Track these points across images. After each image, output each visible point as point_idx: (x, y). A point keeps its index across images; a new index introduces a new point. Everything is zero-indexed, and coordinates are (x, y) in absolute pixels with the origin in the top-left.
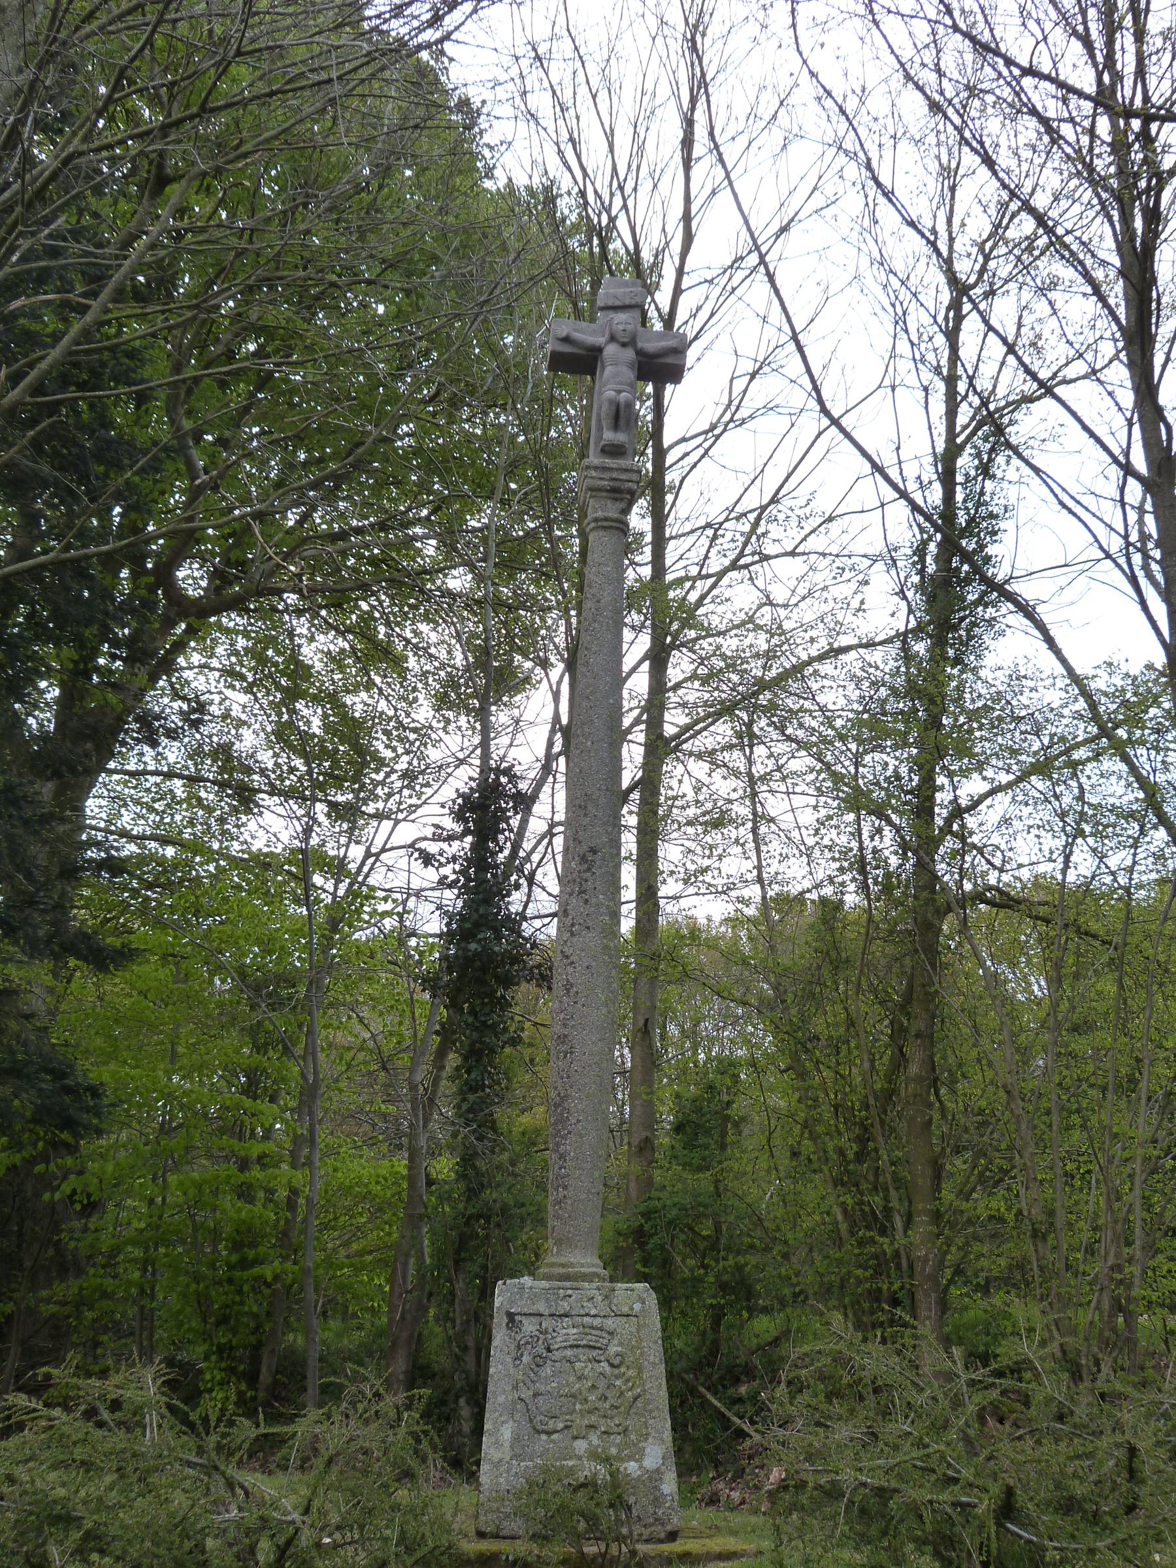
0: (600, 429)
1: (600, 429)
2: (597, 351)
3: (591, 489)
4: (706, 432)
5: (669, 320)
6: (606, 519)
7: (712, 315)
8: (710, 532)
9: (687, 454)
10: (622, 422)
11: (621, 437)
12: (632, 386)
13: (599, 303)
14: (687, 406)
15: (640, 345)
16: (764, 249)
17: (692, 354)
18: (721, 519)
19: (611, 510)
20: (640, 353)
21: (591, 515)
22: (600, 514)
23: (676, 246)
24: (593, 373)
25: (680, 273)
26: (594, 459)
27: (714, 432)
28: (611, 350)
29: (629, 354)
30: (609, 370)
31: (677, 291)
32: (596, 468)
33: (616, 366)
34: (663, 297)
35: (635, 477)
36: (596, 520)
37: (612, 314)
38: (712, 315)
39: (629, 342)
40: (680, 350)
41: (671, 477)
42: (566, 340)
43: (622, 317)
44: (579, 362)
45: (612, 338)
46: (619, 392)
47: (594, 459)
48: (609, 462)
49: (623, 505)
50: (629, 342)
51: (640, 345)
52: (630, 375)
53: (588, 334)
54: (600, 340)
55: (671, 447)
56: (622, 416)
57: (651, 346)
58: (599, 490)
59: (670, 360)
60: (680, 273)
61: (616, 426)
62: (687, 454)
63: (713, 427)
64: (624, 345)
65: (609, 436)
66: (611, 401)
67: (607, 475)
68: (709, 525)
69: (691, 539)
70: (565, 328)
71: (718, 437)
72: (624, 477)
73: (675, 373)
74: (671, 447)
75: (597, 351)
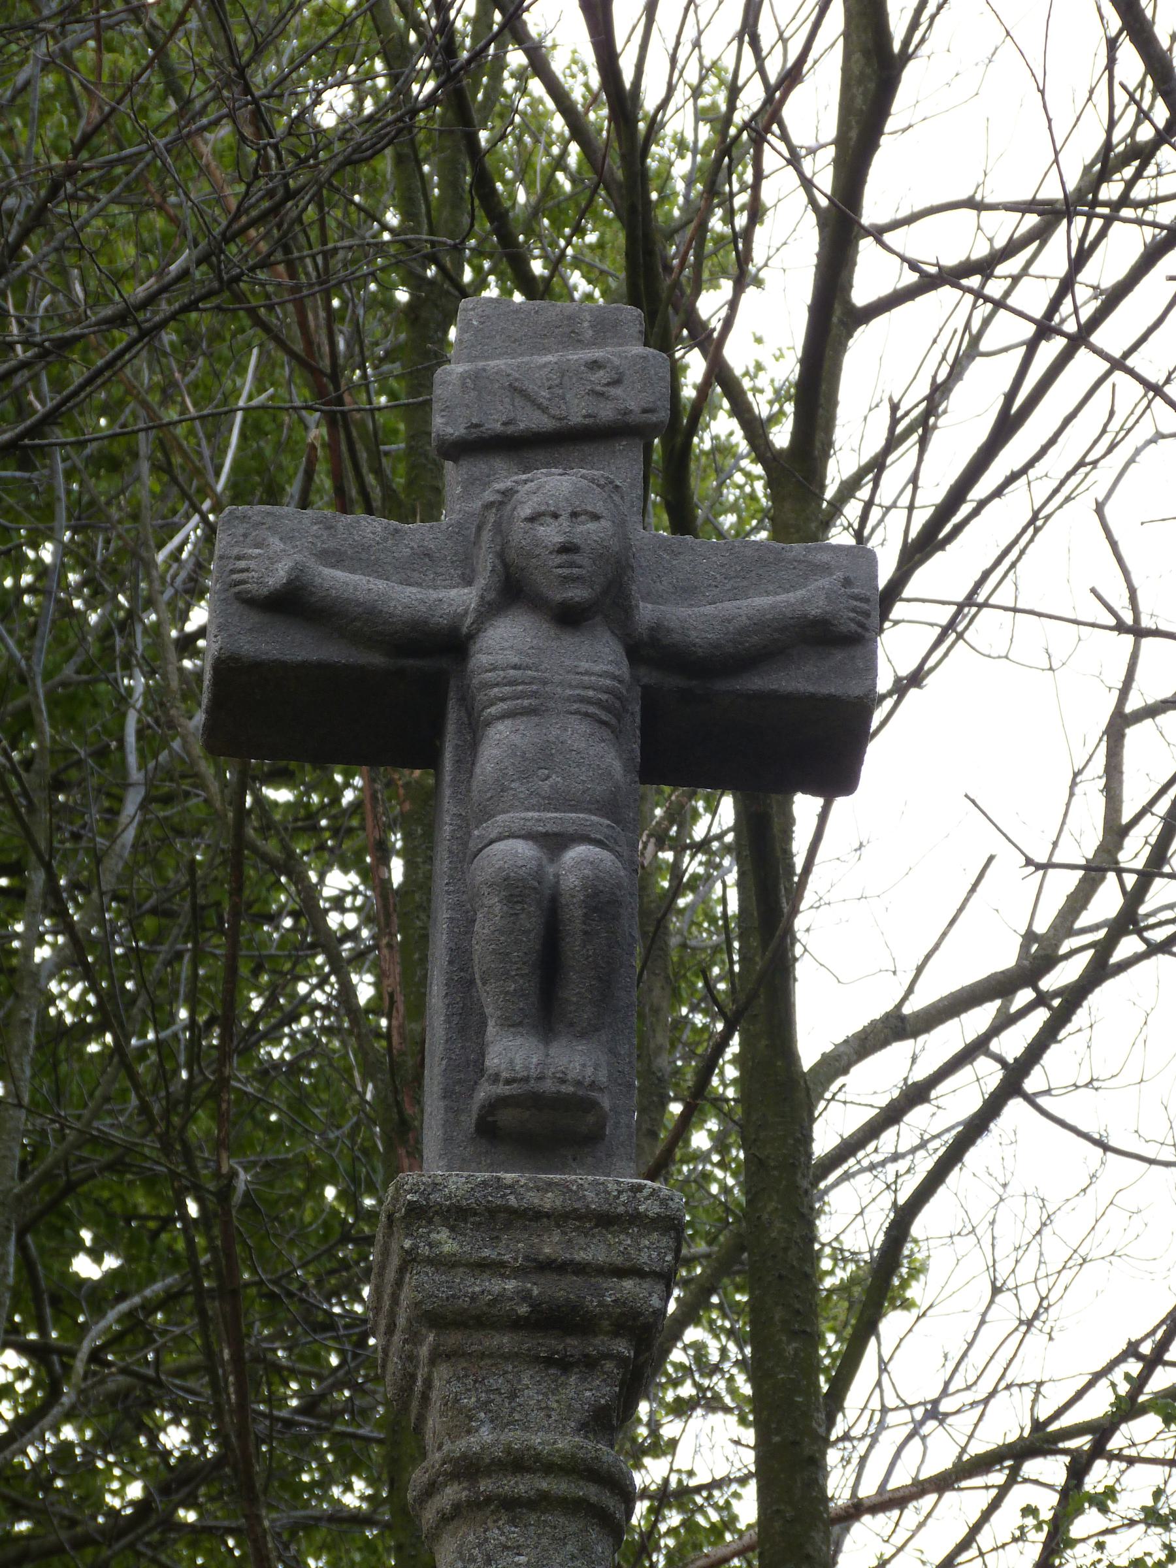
0: (468, 1025)
1: (468, 1025)
2: (450, 645)
3: (435, 1318)
4: (998, 987)
5: (797, 473)
6: (517, 1463)
7: (1007, 425)
8: (1051, 1469)
9: (916, 1094)
10: (576, 988)
11: (574, 1061)
12: (621, 814)
13: (444, 425)
14: (902, 877)
15: (646, 612)
16: (944, 615)
17: (897, 648)
18: (1097, 1405)
19: (543, 1419)
20: (648, 651)
21: (441, 1444)
22: (483, 1437)
23: (814, 113)
24: (431, 760)
25: (841, 229)
26: (443, 1169)
27: (1044, 983)
28: (506, 642)
29: (597, 659)
30: (502, 740)
31: (833, 317)
32: (457, 1215)
33: (536, 718)
34: (764, 331)
35: (650, 1250)
36: (468, 1468)
37: (504, 476)
38: (1007, 425)
39: (592, 601)
40: (846, 627)
41: (849, 1219)
42: (291, 603)
43: (553, 484)
44: (365, 701)
45: (513, 590)
46: (554, 843)
47: (443, 1169)
48: (519, 1182)
49: (595, 1391)
50: (592, 601)
51: (646, 612)
52: (600, 758)
53: (393, 574)
54: (459, 599)
55: (839, 1062)
56: (584, 955)
57: (702, 615)
58: (478, 1319)
59: (797, 679)
60: (841, 229)
61: (546, 1013)
62: (916, 1094)
63: (1038, 956)
64: (569, 618)
65: (510, 1053)
66: (517, 889)
67: (511, 1248)
68: (1039, 1441)
69: (967, 1501)
70: (281, 546)
71: (1075, 995)
72: (595, 1250)
73: (826, 745)
74: (839, 1062)
75: (450, 645)
